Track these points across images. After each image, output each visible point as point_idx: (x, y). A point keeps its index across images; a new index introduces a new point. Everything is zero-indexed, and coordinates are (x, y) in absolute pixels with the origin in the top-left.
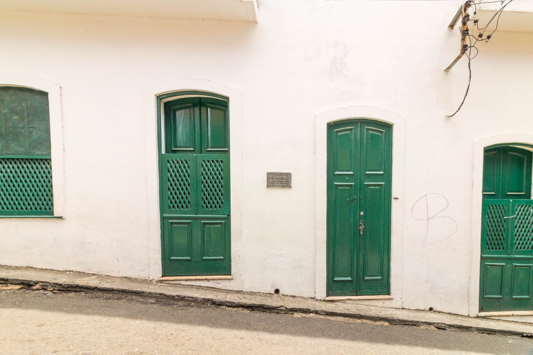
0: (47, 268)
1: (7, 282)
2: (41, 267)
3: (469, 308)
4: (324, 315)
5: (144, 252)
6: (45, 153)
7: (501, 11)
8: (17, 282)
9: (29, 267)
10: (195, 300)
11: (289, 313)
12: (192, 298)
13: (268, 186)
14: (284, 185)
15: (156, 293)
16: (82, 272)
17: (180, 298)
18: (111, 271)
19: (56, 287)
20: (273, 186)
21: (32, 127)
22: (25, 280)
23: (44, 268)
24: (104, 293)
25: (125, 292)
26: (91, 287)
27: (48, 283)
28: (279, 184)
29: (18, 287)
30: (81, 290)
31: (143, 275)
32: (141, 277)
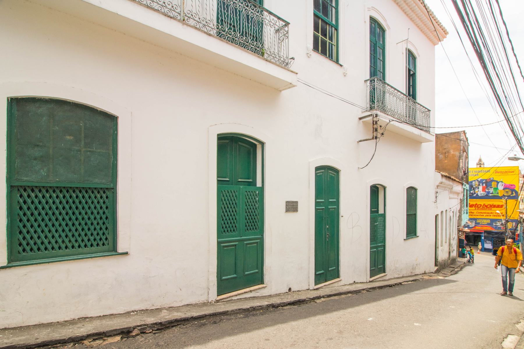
0: (105, 315)
1: (101, 336)
2: (98, 315)
3: (367, 277)
4: (327, 297)
5: (203, 277)
6: (104, 181)
7: (389, 123)
8: (115, 333)
9: (83, 318)
10: (261, 308)
11: (312, 301)
12: (260, 306)
13: (286, 211)
14: (294, 210)
15: (236, 310)
16: (145, 309)
17: (252, 309)
18: (174, 301)
19: (154, 327)
20: (289, 211)
21: (90, 151)
22: (124, 328)
23: (102, 315)
24: (199, 321)
25: (215, 315)
26: (188, 318)
27: (145, 325)
28: (292, 210)
29: (118, 338)
30: (178, 324)
31: (203, 299)
32: (201, 301)
